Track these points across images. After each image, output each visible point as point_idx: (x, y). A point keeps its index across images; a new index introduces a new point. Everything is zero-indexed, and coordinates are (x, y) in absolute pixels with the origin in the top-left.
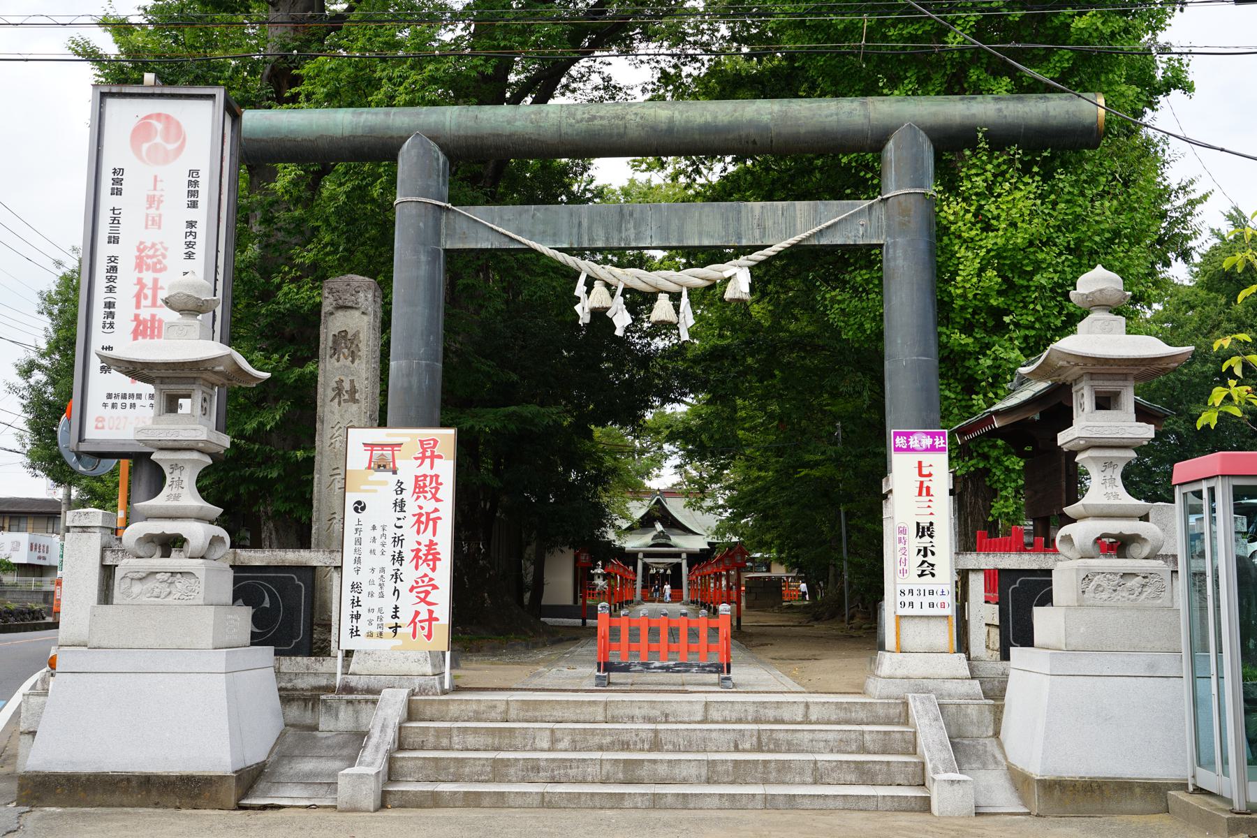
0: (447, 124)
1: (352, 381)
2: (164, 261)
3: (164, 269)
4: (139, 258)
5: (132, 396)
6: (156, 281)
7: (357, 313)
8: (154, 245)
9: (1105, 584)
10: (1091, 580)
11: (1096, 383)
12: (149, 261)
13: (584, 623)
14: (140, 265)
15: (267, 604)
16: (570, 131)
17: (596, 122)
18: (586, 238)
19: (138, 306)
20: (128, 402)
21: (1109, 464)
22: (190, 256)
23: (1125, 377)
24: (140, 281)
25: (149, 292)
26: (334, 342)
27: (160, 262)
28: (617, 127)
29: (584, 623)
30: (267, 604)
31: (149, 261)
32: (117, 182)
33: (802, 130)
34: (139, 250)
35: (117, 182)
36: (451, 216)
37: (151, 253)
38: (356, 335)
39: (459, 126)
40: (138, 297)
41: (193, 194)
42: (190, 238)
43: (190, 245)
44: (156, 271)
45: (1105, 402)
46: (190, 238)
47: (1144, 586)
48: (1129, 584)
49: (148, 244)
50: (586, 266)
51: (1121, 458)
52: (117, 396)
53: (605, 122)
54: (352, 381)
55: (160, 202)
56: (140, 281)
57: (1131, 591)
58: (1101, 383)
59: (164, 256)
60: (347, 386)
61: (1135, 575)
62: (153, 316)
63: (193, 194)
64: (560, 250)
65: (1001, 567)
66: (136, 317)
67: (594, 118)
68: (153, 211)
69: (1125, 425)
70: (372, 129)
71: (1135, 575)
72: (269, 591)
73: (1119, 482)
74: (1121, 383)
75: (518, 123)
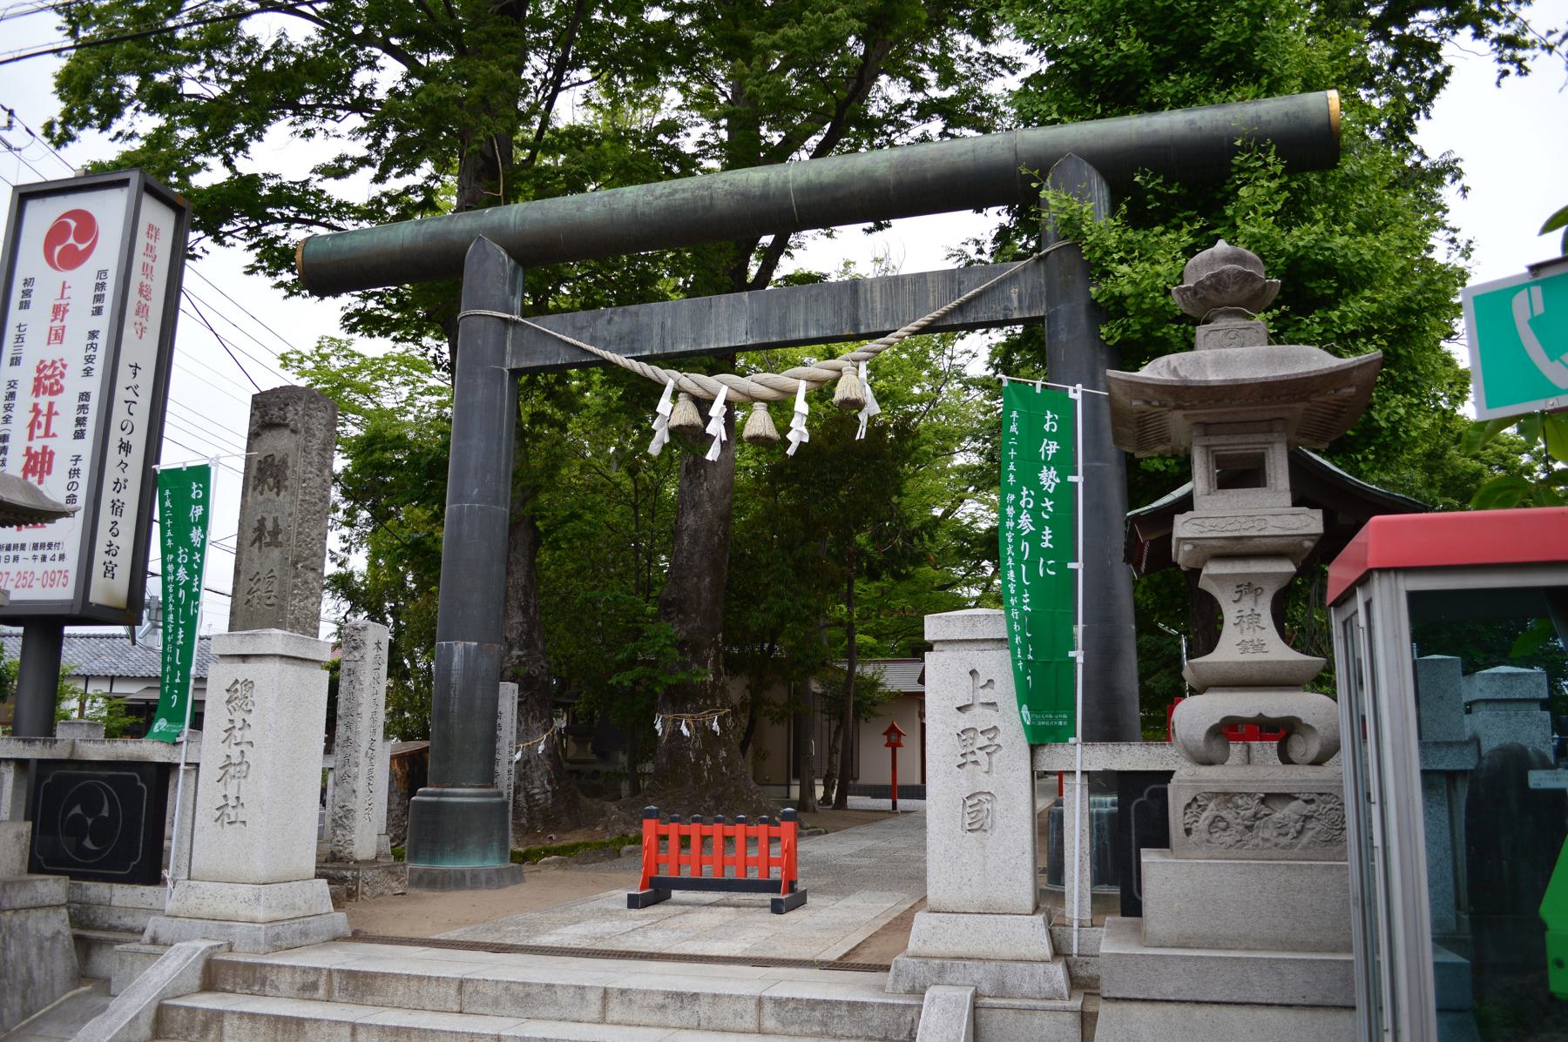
0: (512, 219)
1: (275, 520)
2: (62, 382)
3: (61, 390)
4: (38, 380)
5: (16, 547)
6: (51, 405)
7: (287, 432)
8: (54, 362)
9: (1228, 815)
10: (1203, 808)
11: (1213, 441)
12: (47, 383)
13: (894, 804)
14: (37, 390)
15: (105, 813)
16: (647, 210)
17: (677, 196)
18: (669, 342)
19: (31, 438)
20: (12, 553)
21: (1247, 587)
22: (88, 372)
23: (1268, 426)
24: (35, 406)
25: (43, 419)
26: (259, 470)
27: (57, 382)
28: (702, 198)
29: (894, 804)
30: (105, 813)
31: (47, 383)
32: (27, 293)
33: (929, 175)
34: (39, 371)
35: (27, 293)
36: (519, 330)
37: (49, 372)
38: (284, 461)
39: (524, 220)
40: (32, 426)
41: (99, 298)
42: (91, 352)
43: (89, 359)
44: (52, 393)
45: (1240, 474)
46: (91, 352)
47: (1307, 818)
48: (1278, 815)
49: (48, 363)
50: (671, 378)
51: (1265, 575)
52: (43, 546)
53: (688, 195)
54: (275, 520)
55: (66, 311)
56: (35, 406)
57: (1282, 828)
58: (1223, 439)
59: (62, 375)
60: (269, 525)
61: (1288, 797)
62: (45, 448)
63: (99, 298)
64: (638, 359)
65: (1116, 767)
66: (29, 449)
67: (675, 191)
68: (57, 323)
69: (1274, 512)
70: (433, 236)
71: (1288, 797)
72: (109, 794)
73: (1267, 619)
74: (1261, 438)
75: (588, 209)
